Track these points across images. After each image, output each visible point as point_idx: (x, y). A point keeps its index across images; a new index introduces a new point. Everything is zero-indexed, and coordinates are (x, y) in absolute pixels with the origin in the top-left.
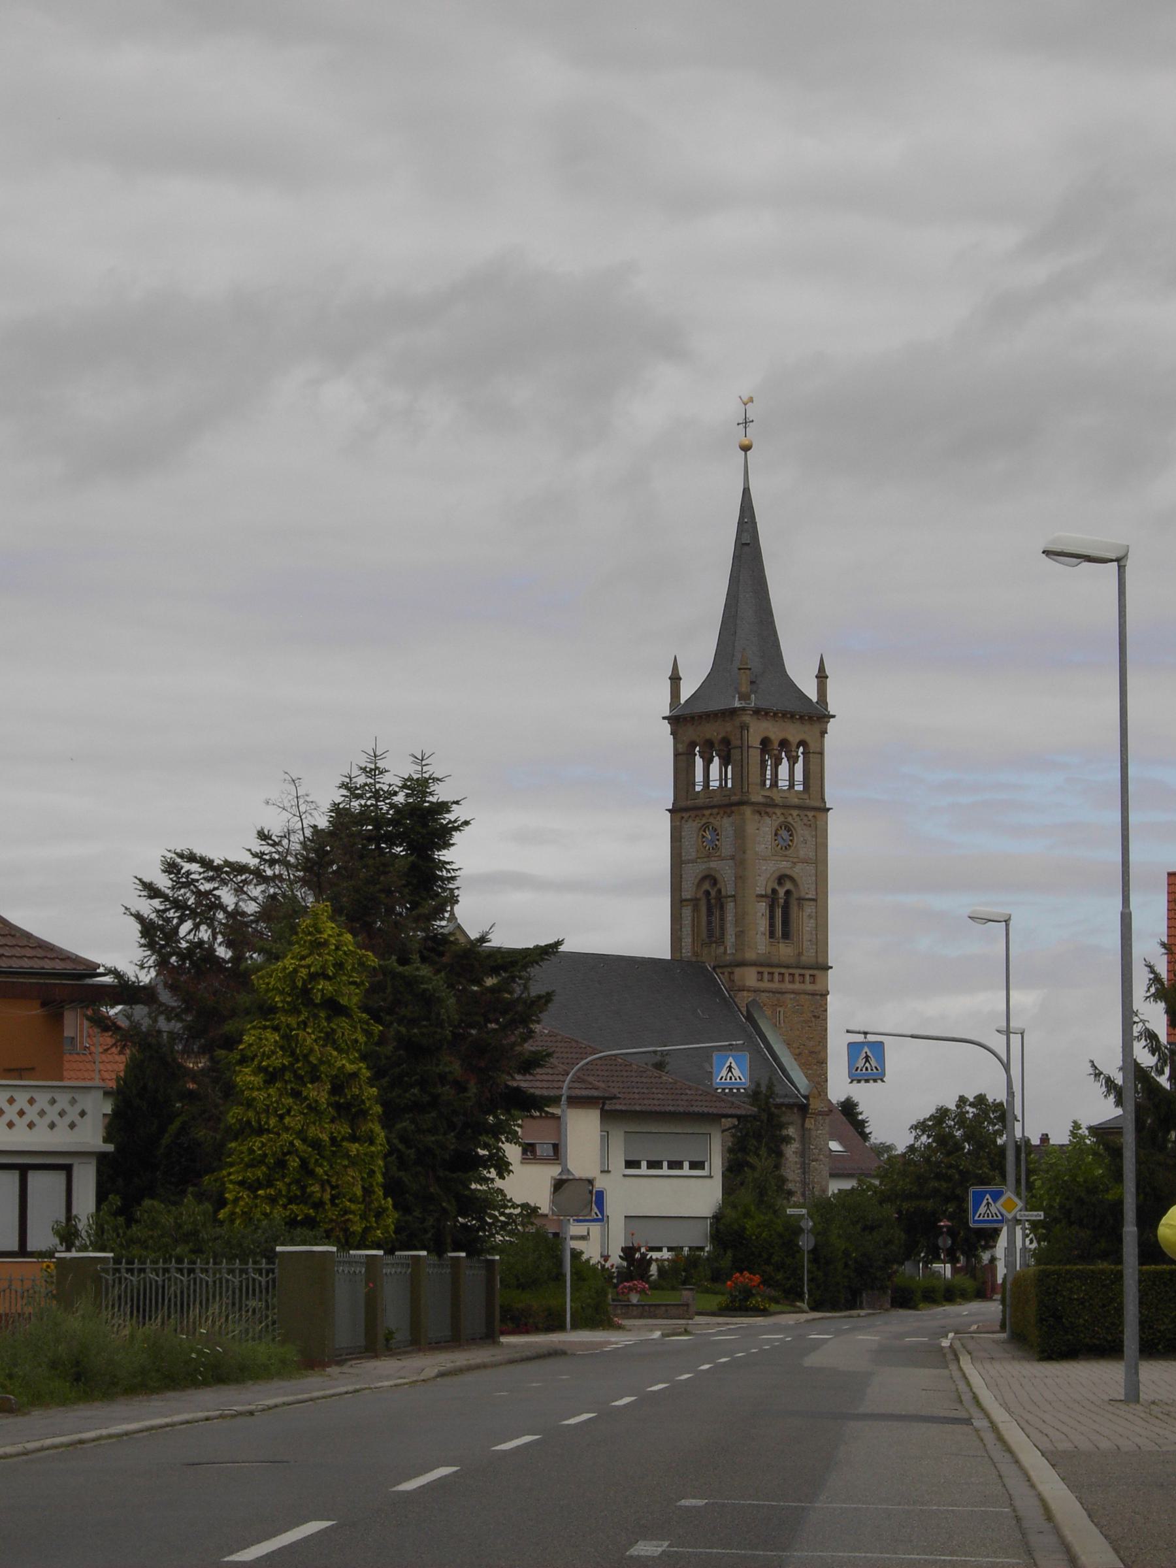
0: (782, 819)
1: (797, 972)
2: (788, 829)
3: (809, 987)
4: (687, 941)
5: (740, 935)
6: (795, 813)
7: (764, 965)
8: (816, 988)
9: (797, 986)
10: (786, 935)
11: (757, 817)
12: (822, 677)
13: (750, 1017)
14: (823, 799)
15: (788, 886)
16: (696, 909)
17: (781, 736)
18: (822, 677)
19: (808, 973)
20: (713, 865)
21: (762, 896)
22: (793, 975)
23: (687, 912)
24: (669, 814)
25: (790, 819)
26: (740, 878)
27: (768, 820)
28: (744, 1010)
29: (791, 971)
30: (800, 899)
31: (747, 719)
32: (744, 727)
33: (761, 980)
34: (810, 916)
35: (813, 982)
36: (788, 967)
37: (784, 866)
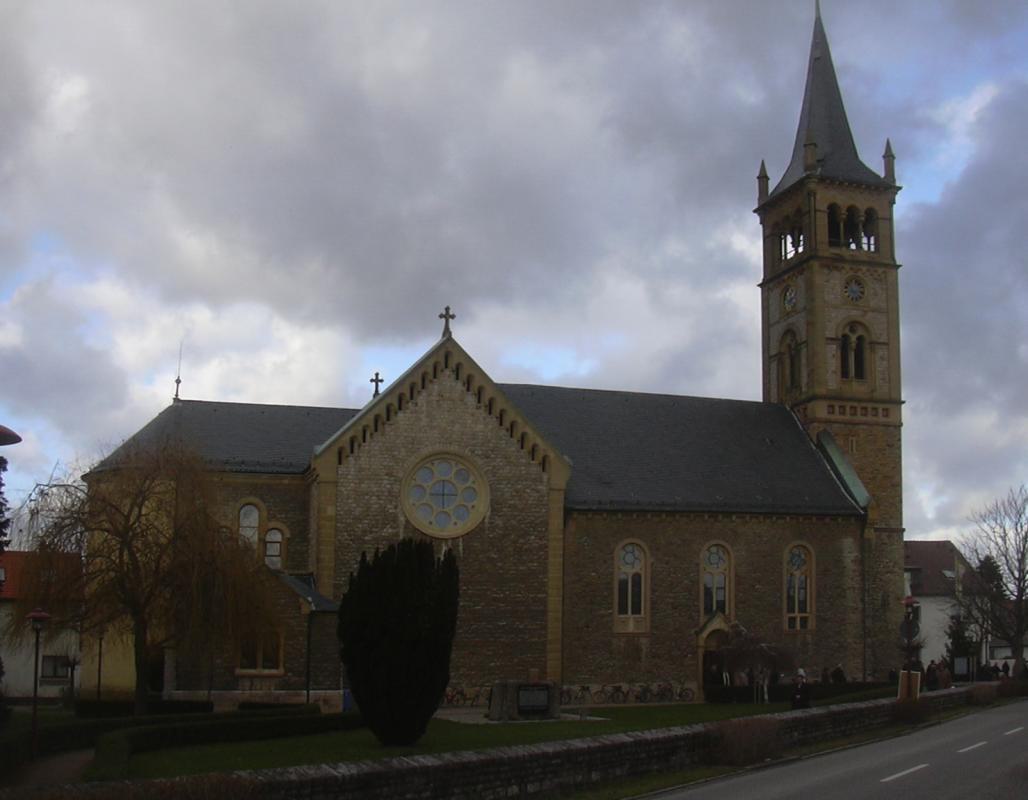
0: (851, 273)
1: (870, 406)
2: (859, 283)
3: (881, 419)
4: (774, 391)
5: (811, 373)
6: (864, 269)
7: (832, 398)
8: (890, 420)
9: (870, 418)
10: (860, 374)
11: (826, 271)
12: (889, 157)
13: (820, 446)
14: (894, 259)
15: (860, 332)
16: (781, 362)
17: (850, 203)
18: (889, 157)
19: (880, 407)
20: (790, 320)
21: (832, 339)
22: (865, 408)
23: (774, 365)
24: (759, 289)
25: (860, 274)
26: (810, 324)
27: (836, 274)
28: (815, 439)
29: (864, 405)
30: (872, 343)
31: (812, 186)
32: (812, 194)
33: (833, 413)
34: (882, 358)
35: (887, 416)
36: (859, 401)
37: (855, 314)
